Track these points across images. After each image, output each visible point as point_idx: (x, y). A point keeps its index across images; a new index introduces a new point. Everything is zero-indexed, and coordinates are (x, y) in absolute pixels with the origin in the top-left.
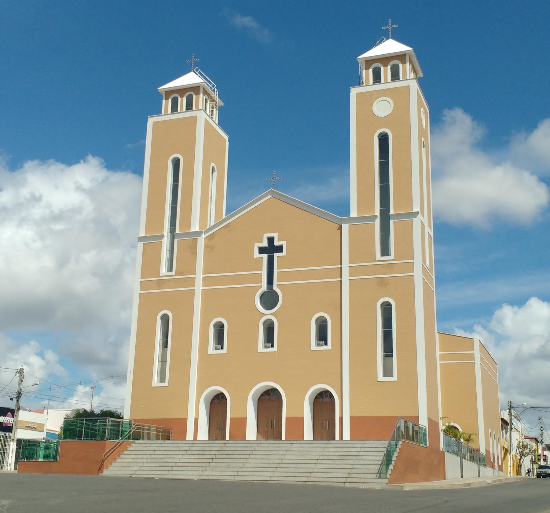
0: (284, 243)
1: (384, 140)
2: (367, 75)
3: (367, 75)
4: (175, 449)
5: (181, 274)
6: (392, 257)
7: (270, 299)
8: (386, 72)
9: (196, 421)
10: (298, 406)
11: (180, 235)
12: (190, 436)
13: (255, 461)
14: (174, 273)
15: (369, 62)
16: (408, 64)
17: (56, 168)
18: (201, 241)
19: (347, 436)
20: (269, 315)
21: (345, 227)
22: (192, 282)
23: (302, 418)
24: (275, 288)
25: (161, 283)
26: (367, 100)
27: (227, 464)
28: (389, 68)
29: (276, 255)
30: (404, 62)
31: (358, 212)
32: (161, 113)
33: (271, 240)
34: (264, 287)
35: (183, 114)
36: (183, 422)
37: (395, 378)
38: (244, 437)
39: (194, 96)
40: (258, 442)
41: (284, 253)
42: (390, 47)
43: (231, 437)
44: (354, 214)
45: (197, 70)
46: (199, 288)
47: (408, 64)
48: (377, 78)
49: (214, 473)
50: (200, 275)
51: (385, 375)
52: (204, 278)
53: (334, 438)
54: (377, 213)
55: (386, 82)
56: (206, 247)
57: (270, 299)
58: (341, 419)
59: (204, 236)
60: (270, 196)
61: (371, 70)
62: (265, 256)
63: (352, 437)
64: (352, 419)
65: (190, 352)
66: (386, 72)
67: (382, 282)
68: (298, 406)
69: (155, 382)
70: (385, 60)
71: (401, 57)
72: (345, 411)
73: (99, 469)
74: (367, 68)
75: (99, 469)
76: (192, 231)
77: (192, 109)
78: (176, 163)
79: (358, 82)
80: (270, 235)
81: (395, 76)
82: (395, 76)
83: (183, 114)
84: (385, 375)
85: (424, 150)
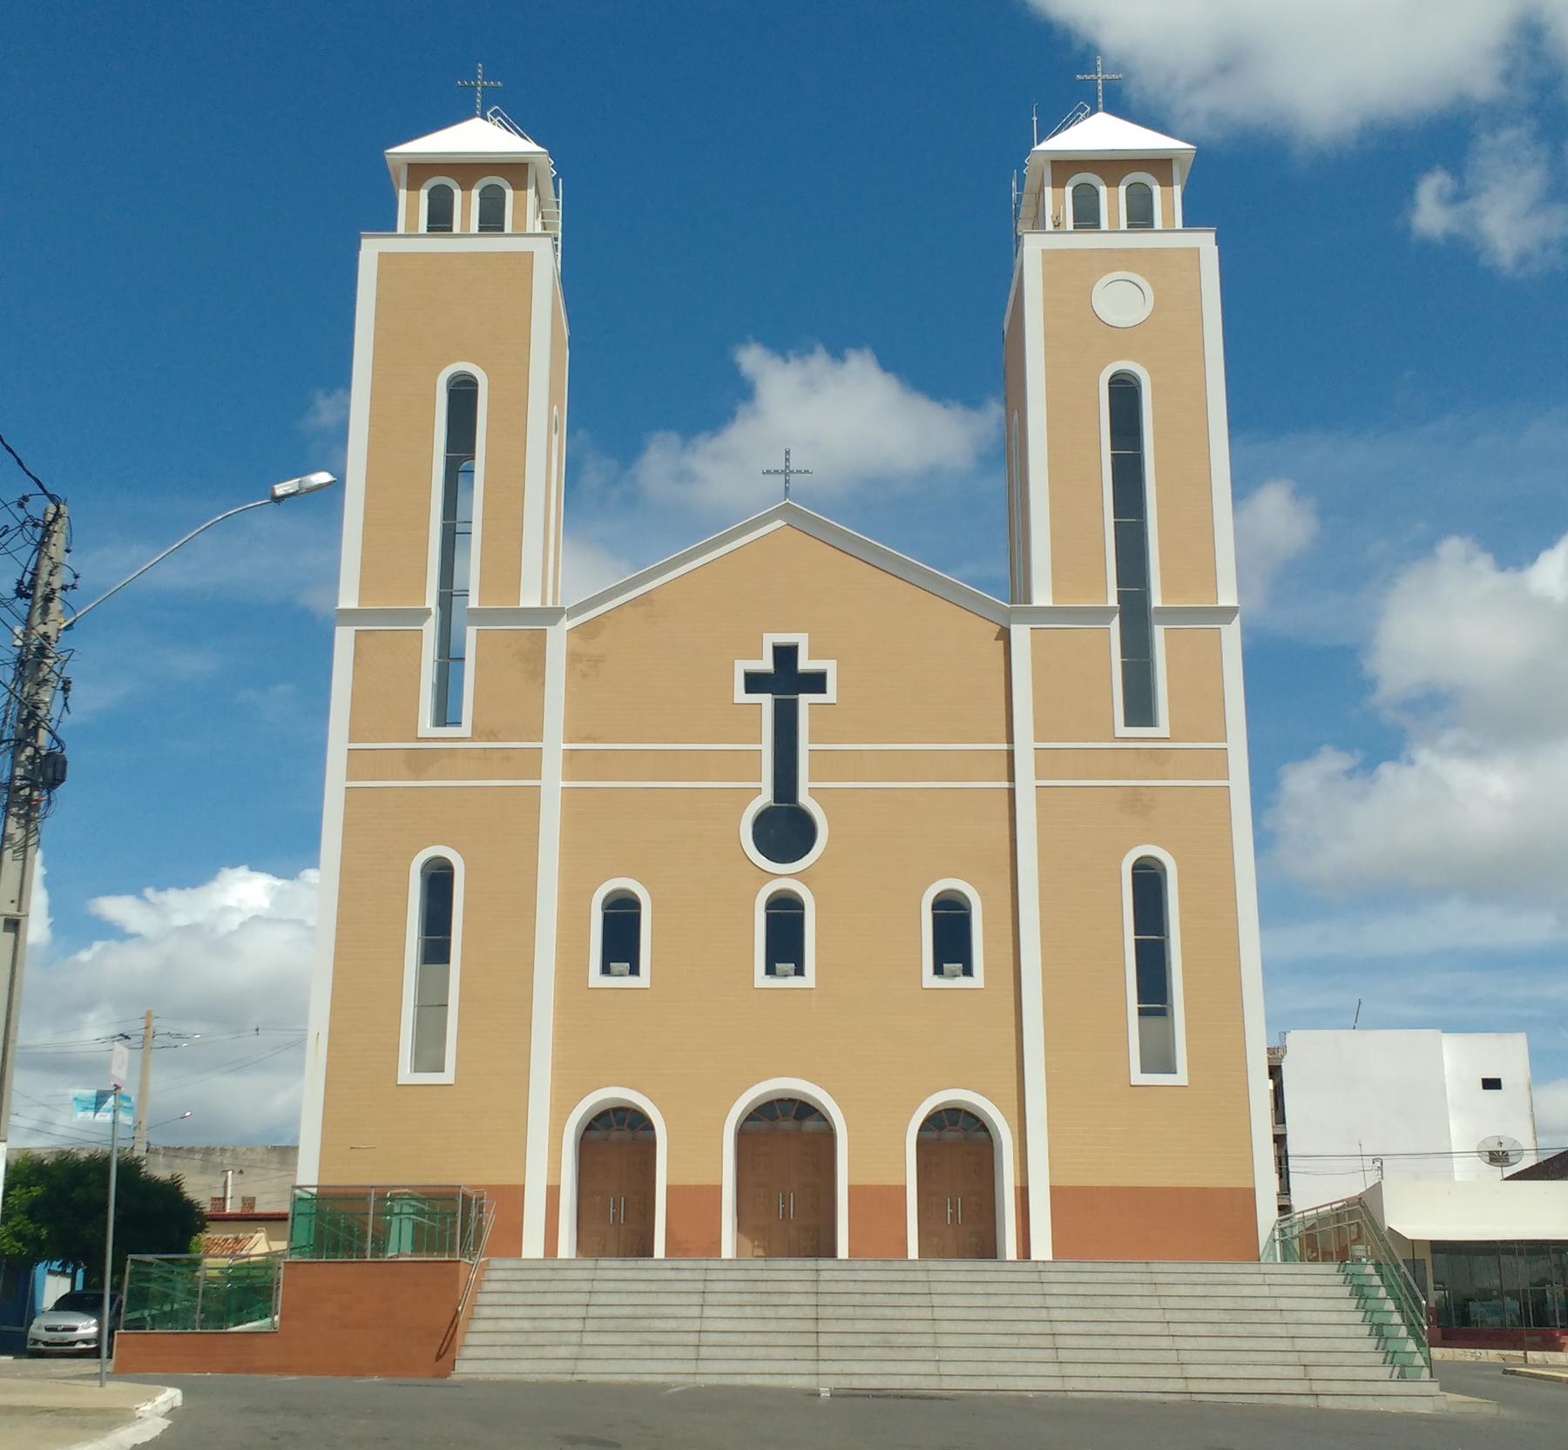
0: (829, 667)
1: (1125, 393)
2: (413, 206)
3: (413, 206)
4: (653, 1287)
5: (492, 735)
6: (1163, 728)
7: (785, 831)
8: (467, 205)
9: (553, 1193)
10: (875, 1153)
11: (478, 616)
12: (533, 1246)
13: (717, 1318)
14: (465, 730)
15: (420, 170)
16: (531, 192)
17: (819, 362)
18: (557, 639)
19: (1042, 1248)
20: (785, 877)
21: (1021, 635)
22: (531, 763)
23: (1251, 1193)
24: (805, 799)
25: (418, 761)
26: (1072, 275)
27: (877, 1338)
28: (1122, 189)
29: (805, 700)
30: (520, 186)
31: (1056, 594)
32: (395, 229)
33: (786, 655)
34: (766, 798)
35: (466, 239)
36: (513, 1196)
37: (1181, 1077)
38: (517, 1252)
39: (509, 193)
40: (743, 1264)
41: (831, 695)
42: (480, 136)
43: (673, 1248)
44: (1042, 596)
45: (495, 114)
46: (553, 783)
47: (531, 192)
48: (440, 220)
49: (857, 1367)
50: (554, 744)
51: (417, 1068)
52: (570, 755)
53: (831, 1253)
54: (432, 602)
55: (1114, 231)
56: (573, 658)
57: (785, 831)
58: (1023, 1194)
59: (567, 624)
60: (779, 523)
61: (1069, 190)
62: (766, 701)
63: (583, 1247)
64: (1056, 1193)
65: (528, 983)
66: (467, 205)
67: (1136, 801)
68: (697, 1154)
69: (406, 1074)
70: (467, 170)
71: (515, 170)
72: (1032, 1169)
73: (439, 1357)
74: (413, 186)
75: (439, 1357)
76: (522, 605)
77: (502, 229)
78: (463, 395)
79: (386, 223)
80: (785, 638)
81: (492, 221)
82: (492, 221)
83: (466, 239)
84: (417, 1068)
85: (555, 438)
